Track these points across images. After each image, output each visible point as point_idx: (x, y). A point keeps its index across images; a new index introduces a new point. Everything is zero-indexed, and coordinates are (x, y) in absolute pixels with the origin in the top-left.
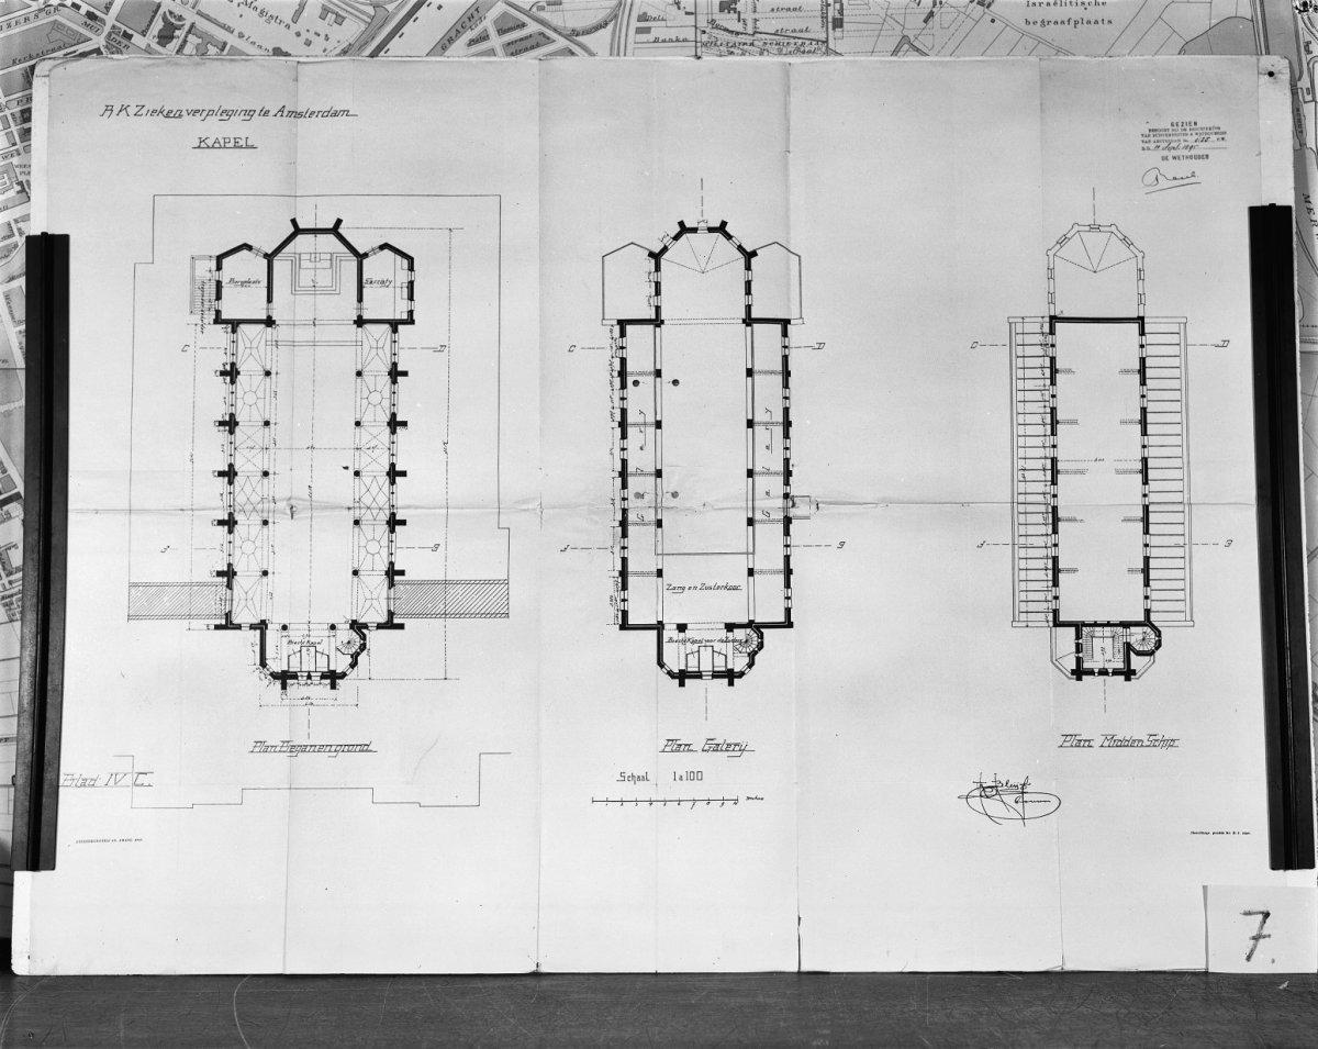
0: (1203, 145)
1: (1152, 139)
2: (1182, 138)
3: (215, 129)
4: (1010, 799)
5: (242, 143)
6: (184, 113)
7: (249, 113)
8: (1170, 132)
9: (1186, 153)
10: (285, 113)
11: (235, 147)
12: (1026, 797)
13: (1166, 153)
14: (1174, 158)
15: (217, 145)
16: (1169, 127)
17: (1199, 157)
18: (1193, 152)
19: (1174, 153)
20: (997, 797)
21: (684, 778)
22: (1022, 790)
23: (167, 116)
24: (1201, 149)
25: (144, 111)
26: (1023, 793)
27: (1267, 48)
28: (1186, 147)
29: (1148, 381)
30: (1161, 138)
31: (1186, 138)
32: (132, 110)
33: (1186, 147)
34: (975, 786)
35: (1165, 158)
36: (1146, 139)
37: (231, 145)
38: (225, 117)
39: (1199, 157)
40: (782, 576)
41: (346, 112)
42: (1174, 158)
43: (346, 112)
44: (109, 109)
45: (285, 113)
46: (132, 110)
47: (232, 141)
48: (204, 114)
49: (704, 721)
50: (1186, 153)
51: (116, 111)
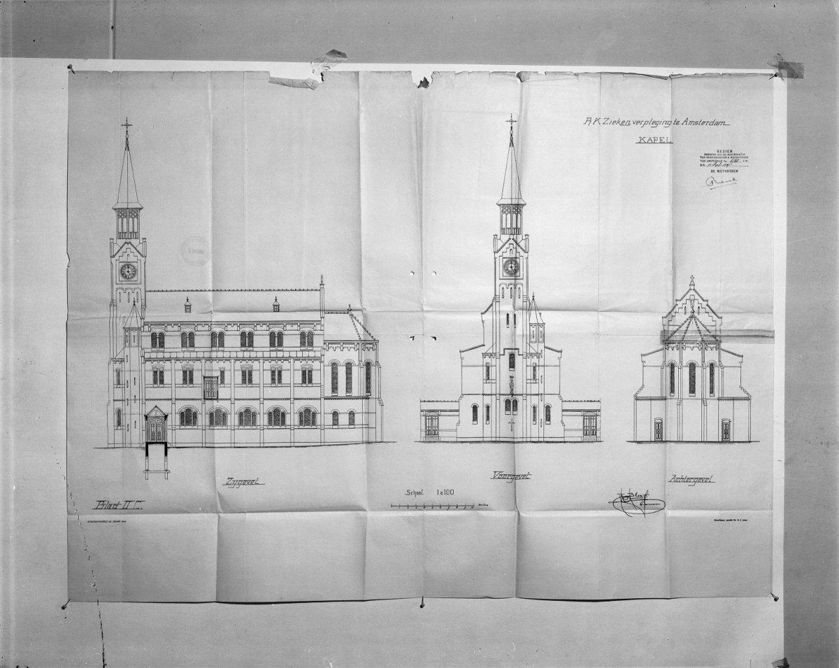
1: (706, 159)
2: (723, 159)
3: (647, 132)
4: (637, 503)
5: (664, 140)
6: (631, 123)
8: (717, 156)
9: (725, 168)
10: (688, 122)
11: (660, 143)
13: (714, 168)
14: (718, 171)
15: (650, 141)
16: (716, 153)
17: (733, 171)
18: (729, 168)
19: (719, 168)
20: (630, 502)
23: (622, 124)
24: (734, 166)
26: (645, 500)
27: (114, 53)
28: (725, 165)
30: (711, 159)
31: (726, 160)
33: (725, 165)
35: (712, 171)
36: (702, 159)
39: (733, 171)
40: (516, 445)
42: (718, 171)
44: (589, 120)
45: (688, 122)
46: (602, 121)
47: (659, 139)
50: (725, 168)
51: (593, 121)
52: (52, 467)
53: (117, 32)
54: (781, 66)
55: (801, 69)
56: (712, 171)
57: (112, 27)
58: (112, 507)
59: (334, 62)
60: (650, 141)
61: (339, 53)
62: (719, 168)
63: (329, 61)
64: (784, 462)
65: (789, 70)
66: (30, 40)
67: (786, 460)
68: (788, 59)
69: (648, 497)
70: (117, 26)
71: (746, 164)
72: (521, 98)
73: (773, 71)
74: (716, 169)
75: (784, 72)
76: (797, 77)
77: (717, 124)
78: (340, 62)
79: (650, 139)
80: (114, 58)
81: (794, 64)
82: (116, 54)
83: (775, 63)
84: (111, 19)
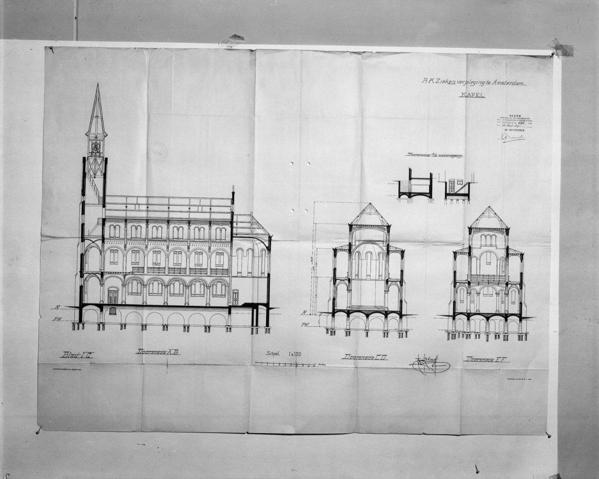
0: (522, 125)
2: (514, 122)
4: (430, 365)
5: (479, 95)
6: (456, 82)
7: (483, 83)
11: (476, 97)
12: (437, 364)
14: (510, 130)
15: (469, 96)
17: (520, 130)
18: (519, 128)
19: (511, 128)
21: (294, 355)
22: (435, 361)
24: (521, 127)
25: (440, 81)
26: (435, 362)
27: (77, 36)
29: (106, 205)
32: (435, 81)
34: (416, 360)
35: (506, 130)
37: (475, 96)
38: (473, 84)
39: (520, 130)
41: (522, 84)
42: (510, 130)
43: (522, 84)
44: (426, 79)
46: (435, 81)
47: (475, 95)
48: (465, 83)
49: (50, 308)
50: (515, 128)
52: (30, 323)
53: (79, 21)
54: (557, 48)
55: (572, 49)
56: (506, 130)
57: (76, 18)
58: (74, 356)
59: (236, 43)
60: (469, 96)
61: (239, 37)
62: (511, 128)
63: (232, 43)
64: (558, 333)
65: (565, 51)
66: (18, 28)
67: (560, 331)
68: (561, 43)
69: (437, 361)
70: (79, 18)
71: (530, 125)
72: (362, 128)
73: (549, 52)
74: (508, 128)
75: (560, 52)
76: (569, 55)
77: (518, 84)
78: (240, 43)
79: (469, 94)
80: (77, 40)
81: (566, 46)
82: (79, 37)
83: (554, 45)
84: (75, 12)
